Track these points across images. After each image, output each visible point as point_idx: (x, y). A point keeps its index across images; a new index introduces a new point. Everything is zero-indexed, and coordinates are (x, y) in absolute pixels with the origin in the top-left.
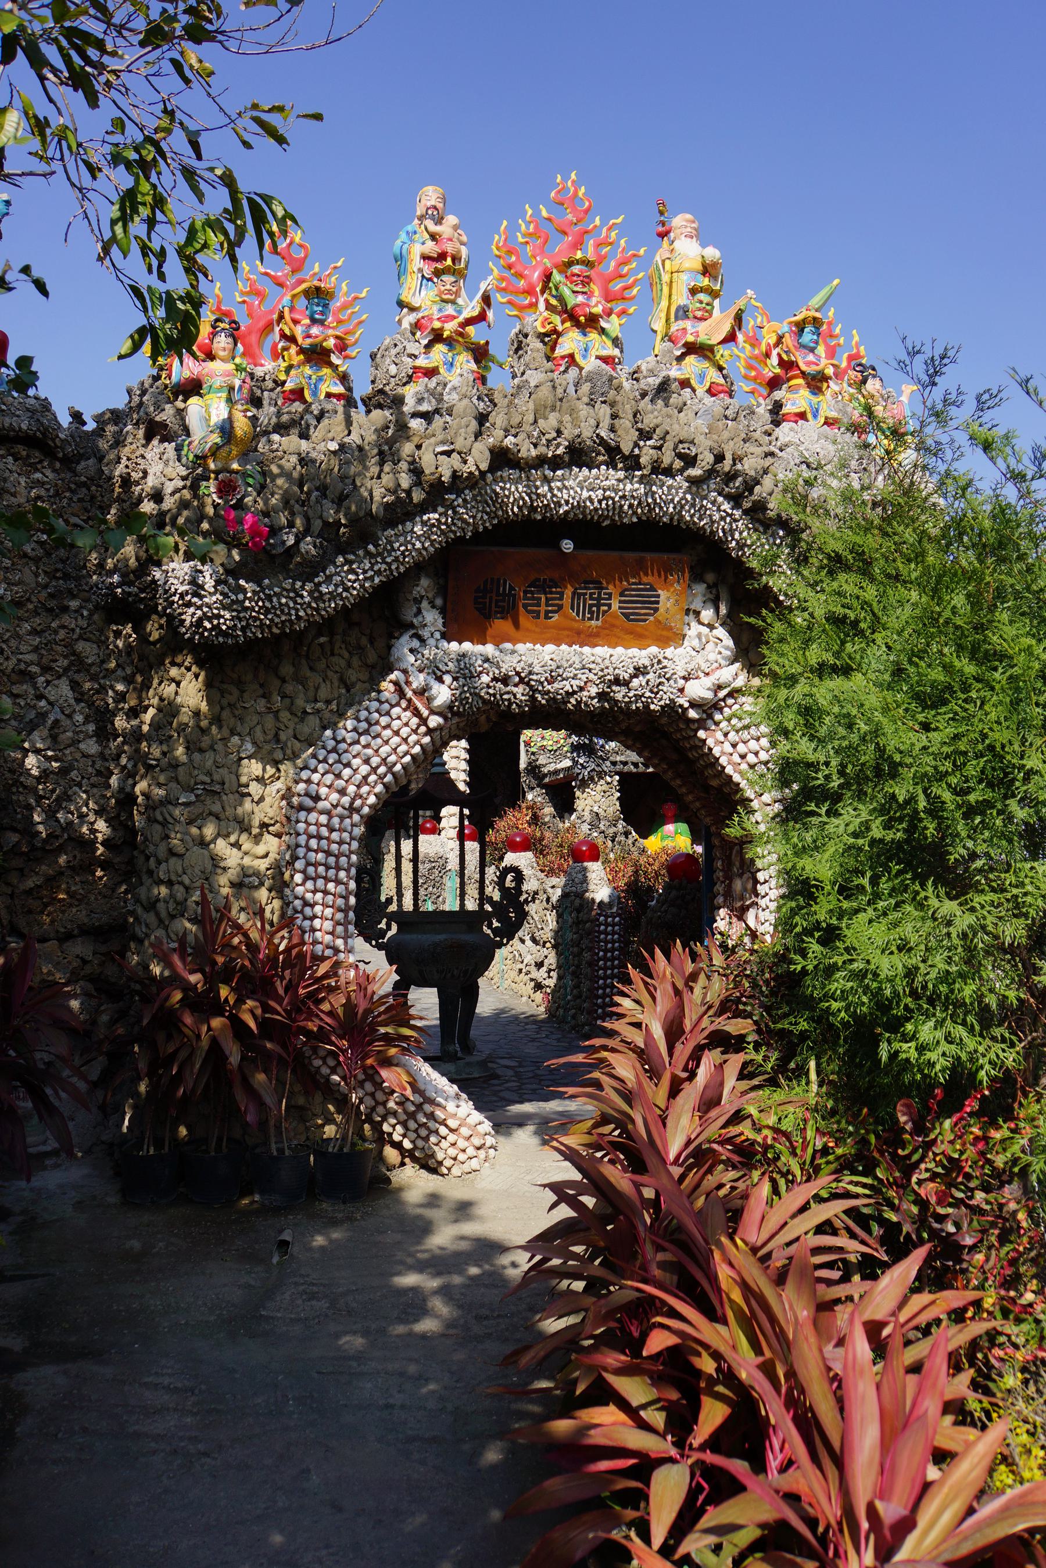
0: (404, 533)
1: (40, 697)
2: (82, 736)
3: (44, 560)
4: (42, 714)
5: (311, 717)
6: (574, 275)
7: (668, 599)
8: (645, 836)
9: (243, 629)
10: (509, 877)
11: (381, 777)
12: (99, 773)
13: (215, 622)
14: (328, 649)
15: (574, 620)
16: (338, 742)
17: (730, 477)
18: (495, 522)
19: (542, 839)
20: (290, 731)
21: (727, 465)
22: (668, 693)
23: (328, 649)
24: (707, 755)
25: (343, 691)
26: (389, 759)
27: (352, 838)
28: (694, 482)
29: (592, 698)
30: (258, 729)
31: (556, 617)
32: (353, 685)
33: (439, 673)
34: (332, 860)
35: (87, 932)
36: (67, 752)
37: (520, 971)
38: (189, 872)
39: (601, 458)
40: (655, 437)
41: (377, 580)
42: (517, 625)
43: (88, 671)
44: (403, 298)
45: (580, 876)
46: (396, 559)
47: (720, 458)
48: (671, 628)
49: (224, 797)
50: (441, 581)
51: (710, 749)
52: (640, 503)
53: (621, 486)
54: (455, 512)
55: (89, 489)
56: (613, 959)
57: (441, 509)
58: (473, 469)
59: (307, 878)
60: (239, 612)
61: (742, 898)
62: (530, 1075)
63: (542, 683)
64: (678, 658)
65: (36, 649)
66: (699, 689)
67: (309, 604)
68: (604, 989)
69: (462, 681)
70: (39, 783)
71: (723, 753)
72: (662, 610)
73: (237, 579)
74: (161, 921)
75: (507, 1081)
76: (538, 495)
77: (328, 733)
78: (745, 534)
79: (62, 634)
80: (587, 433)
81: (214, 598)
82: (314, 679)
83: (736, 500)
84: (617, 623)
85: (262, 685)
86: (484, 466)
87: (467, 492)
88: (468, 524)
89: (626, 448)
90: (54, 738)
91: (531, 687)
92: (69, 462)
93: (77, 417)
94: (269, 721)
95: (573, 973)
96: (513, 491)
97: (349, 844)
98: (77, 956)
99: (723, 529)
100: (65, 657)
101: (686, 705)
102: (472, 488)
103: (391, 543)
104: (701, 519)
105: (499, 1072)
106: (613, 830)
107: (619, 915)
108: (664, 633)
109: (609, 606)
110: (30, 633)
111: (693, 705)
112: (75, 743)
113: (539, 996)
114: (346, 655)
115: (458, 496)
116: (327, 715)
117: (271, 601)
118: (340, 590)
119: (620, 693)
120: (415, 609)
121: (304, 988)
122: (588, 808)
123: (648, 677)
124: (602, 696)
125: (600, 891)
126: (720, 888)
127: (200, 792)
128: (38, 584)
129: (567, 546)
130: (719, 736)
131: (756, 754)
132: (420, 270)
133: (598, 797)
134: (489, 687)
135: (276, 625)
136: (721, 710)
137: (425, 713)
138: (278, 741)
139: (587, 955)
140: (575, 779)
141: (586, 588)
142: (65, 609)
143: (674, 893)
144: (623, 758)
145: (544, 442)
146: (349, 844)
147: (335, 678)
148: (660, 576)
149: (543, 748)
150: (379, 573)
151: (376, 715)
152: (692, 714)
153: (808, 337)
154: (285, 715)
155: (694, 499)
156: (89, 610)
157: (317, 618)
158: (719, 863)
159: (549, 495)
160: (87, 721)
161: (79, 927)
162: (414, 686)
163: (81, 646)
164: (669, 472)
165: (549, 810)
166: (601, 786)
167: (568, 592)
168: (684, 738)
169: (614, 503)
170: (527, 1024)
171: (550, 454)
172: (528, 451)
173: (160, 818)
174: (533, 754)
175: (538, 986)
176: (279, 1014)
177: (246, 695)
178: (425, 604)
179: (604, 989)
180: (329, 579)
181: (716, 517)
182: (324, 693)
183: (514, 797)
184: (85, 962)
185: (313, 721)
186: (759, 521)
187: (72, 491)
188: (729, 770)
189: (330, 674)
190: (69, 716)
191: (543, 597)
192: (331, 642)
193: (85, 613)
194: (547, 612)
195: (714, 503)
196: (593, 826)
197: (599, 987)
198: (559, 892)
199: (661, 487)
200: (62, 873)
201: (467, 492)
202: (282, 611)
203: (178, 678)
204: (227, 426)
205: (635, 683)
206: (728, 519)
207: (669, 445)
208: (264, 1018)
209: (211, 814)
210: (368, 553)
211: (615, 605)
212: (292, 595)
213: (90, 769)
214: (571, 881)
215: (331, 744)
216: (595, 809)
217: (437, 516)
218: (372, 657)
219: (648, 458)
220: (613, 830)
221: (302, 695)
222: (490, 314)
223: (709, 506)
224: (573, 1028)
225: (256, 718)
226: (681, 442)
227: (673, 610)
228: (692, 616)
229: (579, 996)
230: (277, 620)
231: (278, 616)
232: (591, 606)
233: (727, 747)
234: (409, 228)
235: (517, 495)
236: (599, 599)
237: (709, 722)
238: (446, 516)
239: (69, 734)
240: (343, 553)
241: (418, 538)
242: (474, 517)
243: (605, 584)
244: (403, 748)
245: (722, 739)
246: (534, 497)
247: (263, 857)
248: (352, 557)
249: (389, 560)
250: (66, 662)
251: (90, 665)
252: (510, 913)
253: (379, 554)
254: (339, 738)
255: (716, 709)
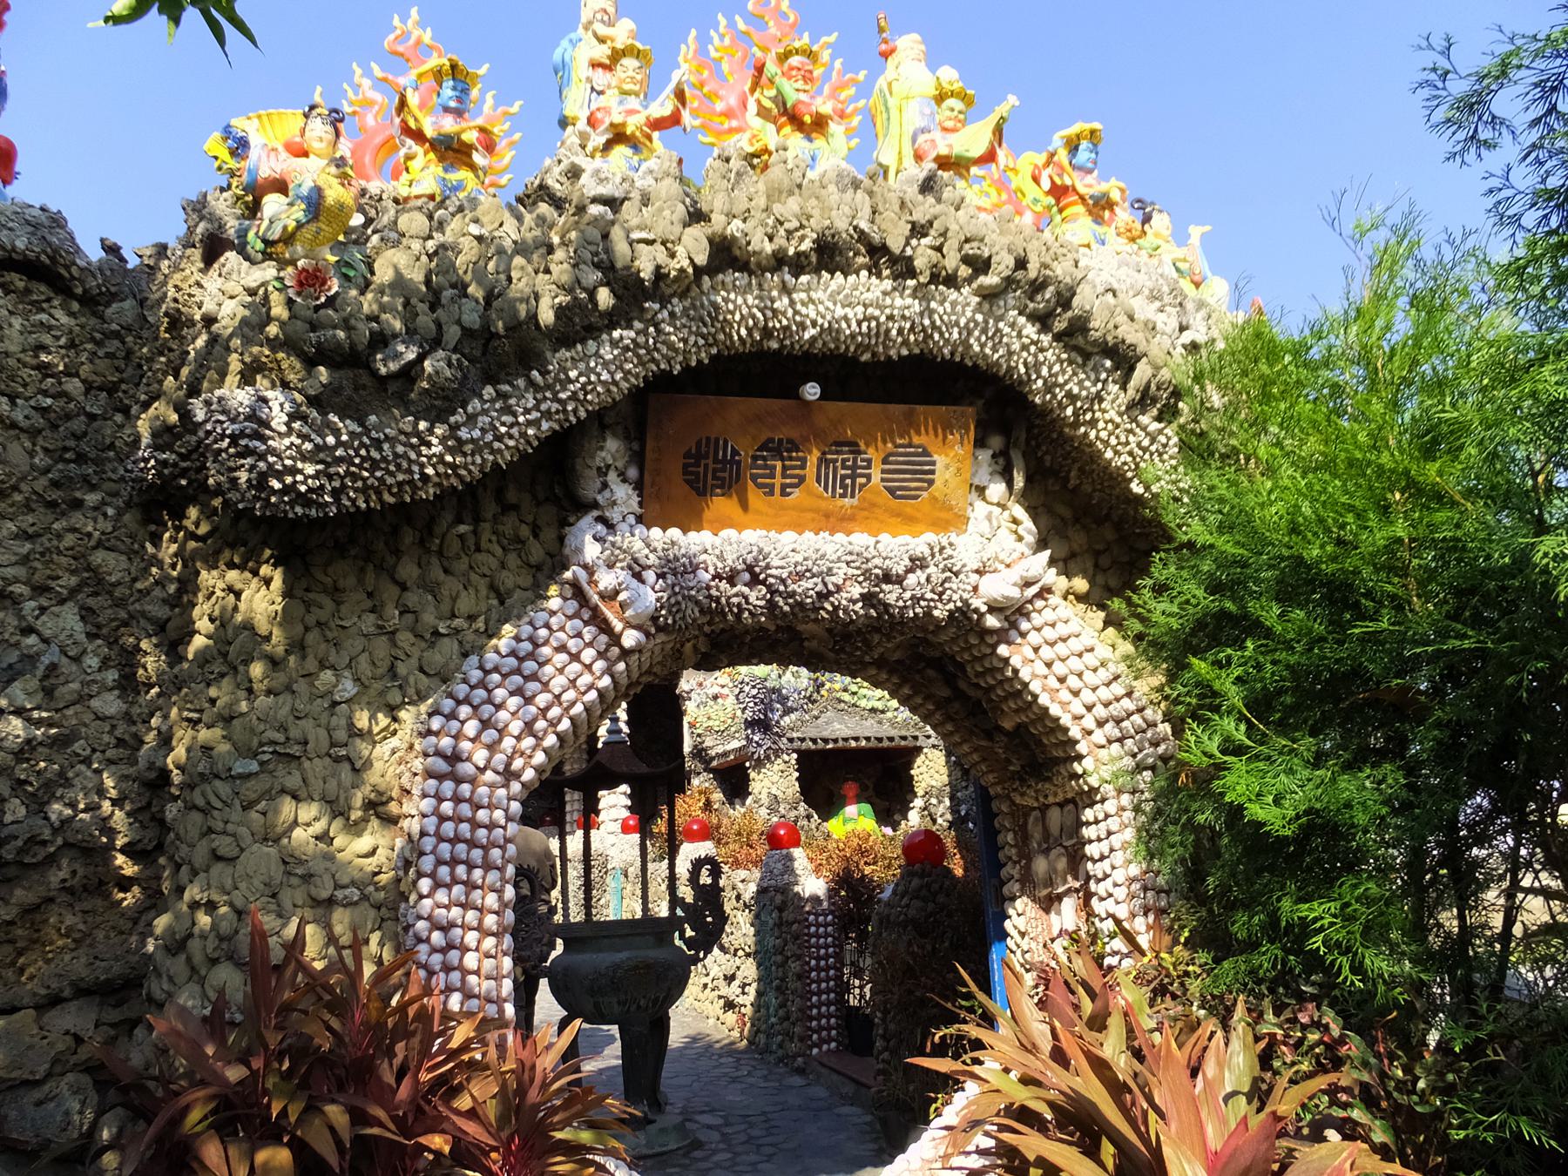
0: (586, 358)
1: (28, 630)
2: (95, 688)
3: (47, 433)
4: (30, 657)
5: (446, 640)
6: (792, 69)
7: (947, 467)
8: (826, 820)
9: (335, 493)
10: (704, 872)
11: (553, 724)
12: (120, 742)
13: (289, 480)
14: (471, 542)
15: (821, 497)
16: (487, 672)
17: (1037, 287)
18: (714, 351)
19: (719, 827)
20: (414, 662)
21: (1033, 271)
22: (958, 591)
23: (471, 542)
24: (1010, 680)
25: (495, 602)
26: (565, 697)
27: (509, 819)
28: (989, 297)
29: (855, 602)
30: (364, 658)
31: (796, 492)
32: (509, 593)
33: (638, 569)
34: (477, 854)
35: (83, 991)
36: (70, 712)
37: (705, 986)
38: (243, 885)
39: (860, 260)
40: (933, 232)
41: (545, 426)
42: (744, 505)
43: (110, 593)
44: (567, 113)
45: (779, 866)
46: (574, 396)
47: (1021, 264)
48: (951, 508)
49: (307, 764)
50: (636, 446)
51: (1016, 671)
52: (912, 329)
53: (888, 301)
54: (659, 331)
55: (123, 343)
56: (828, 968)
57: (638, 325)
58: (685, 263)
59: (437, 885)
60: (328, 465)
61: (1050, 882)
62: (743, 1137)
63: (783, 581)
64: (967, 548)
65: (25, 560)
66: (1000, 586)
67: (441, 457)
68: (819, 1008)
69: (670, 579)
70: (19, 760)
71: (1034, 676)
72: (938, 483)
73: (324, 414)
74: (193, 969)
75: (715, 1152)
76: (774, 311)
77: (474, 659)
78: (1057, 368)
79: (69, 540)
80: (842, 224)
81: (287, 442)
82: (450, 585)
83: (1043, 320)
84: (880, 501)
85: (370, 595)
86: (702, 259)
87: (675, 300)
88: (676, 350)
89: (895, 245)
90: (49, 692)
91: (769, 587)
92: (92, 303)
93: (112, 249)
94: (381, 647)
95: (778, 988)
96: (741, 305)
97: (504, 828)
98: (67, 1033)
99: (1025, 364)
100: (73, 572)
101: (984, 609)
102: (683, 295)
103: (565, 371)
104: (995, 350)
105: (702, 1136)
106: (793, 813)
107: (832, 912)
108: (943, 515)
109: (869, 477)
110: (16, 537)
111: (993, 609)
112: (82, 699)
113: (731, 1018)
114: (499, 551)
115: (663, 307)
116: (469, 636)
117: (380, 450)
118: (489, 437)
119: (891, 594)
120: (598, 485)
121: (430, 1070)
122: (765, 791)
123: (928, 571)
124: (868, 599)
125: (812, 885)
126: (1012, 870)
127: (266, 757)
128: (33, 467)
129: (812, 391)
130: (1030, 654)
131: (1080, 675)
132: (589, 80)
133: (776, 778)
134: (708, 588)
135: (390, 487)
136: (1027, 616)
137: (618, 626)
138: (394, 676)
139: (794, 966)
140: (750, 758)
141: (837, 453)
142: (78, 504)
143: (916, 882)
144: (799, 735)
145: (782, 232)
146: (504, 828)
147: (482, 584)
148: (936, 435)
149: (709, 729)
150: (547, 415)
151: (543, 632)
152: (992, 621)
153: (1084, 155)
154: (405, 638)
155: (986, 322)
156: (117, 508)
157: (454, 481)
158: (1010, 837)
159: (790, 313)
160: (105, 664)
161: (73, 984)
162: (601, 586)
163: (99, 557)
164: (951, 281)
165: (718, 796)
166: (778, 765)
167: (813, 458)
168: (976, 659)
169: (878, 325)
170: (721, 1056)
171: (791, 252)
172: (762, 245)
173: (200, 802)
174: (699, 735)
175: (730, 1005)
176: (381, 1125)
177: (343, 608)
178: (612, 477)
179: (819, 1008)
180: (471, 419)
181: (1016, 346)
182: (465, 604)
183: (677, 782)
184: (79, 1040)
185: (449, 647)
186: (1076, 348)
187: (99, 344)
188: (1044, 700)
189: (474, 577)
190: (76, 660)
191: (779, 464)
192: (475, 532)
193: (110, 511)
194: (784, 487)
195: (1012, 325)
196: (772, 810)
197: (813, 1006)
198: (753, 888)
199: (942, 303)
200: (51, 900)
201: (675, 300)
202: (398, 466)
203: (238, 586)
204: (315, 196)
205: (911, 580)
206: (1033, 349)
207: (951, 248)
208: (358, 1140)
209: (283, 791)
210: (531, 383)
211: (876, 476)
212: (414, 440)
213: (106, 738)
214: (768, 873)
215: (476, 675)
216: (774, 791)
217: (632, 334)
218: (536, 552)
219: (925, 260)
220: (793, 813)
221: (431, 609)
222: (686, 116)
223: (1007, 330)
224: (781, 1060)
225: (359, 643)
226: (967, 240)
227: (953, 482)
228: (974, 495)
229: (787, 1018)
230: (390, 480)
231: (392, 474)
232: (844, 477)
233: (1041, 669)
234: (573, 36)
235: (745, 311)
236: (854, 467)
237: (1013, 633)
238: (646, 334)
239: (75, 686)
240: (494, 381)
241: (606, 364)
242: (685, 341)
243: (863, 447)
244: (587, 679)
245: (1031, 655)
246: (769, 314)
247: (366, 856)
248: (506, 388)
249: (563, 396)
250: (74, 581)
251: (113, 585)
252: (705, 916)
253: (549, 387)
254: (489, 666)
255: (1022, 615)
